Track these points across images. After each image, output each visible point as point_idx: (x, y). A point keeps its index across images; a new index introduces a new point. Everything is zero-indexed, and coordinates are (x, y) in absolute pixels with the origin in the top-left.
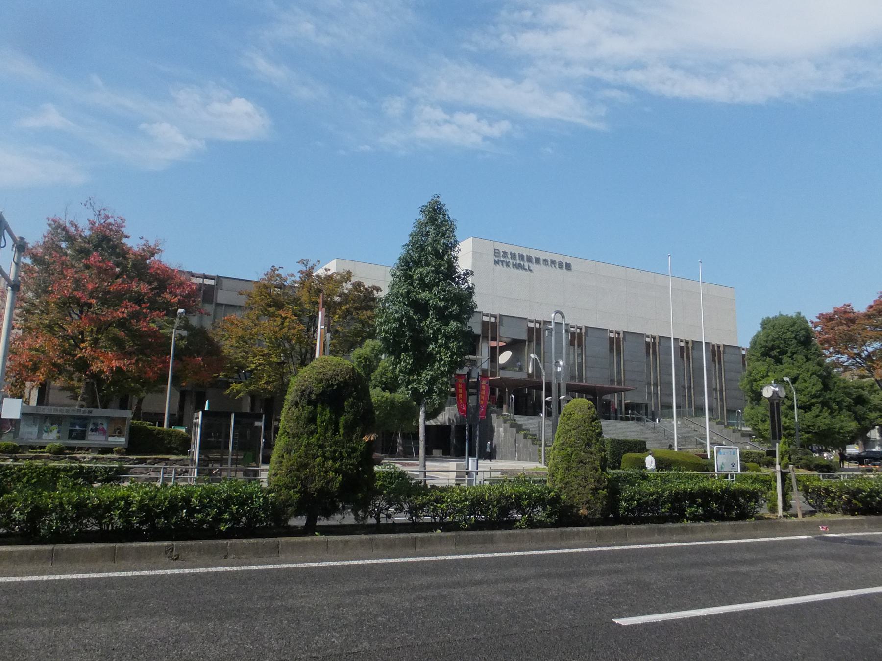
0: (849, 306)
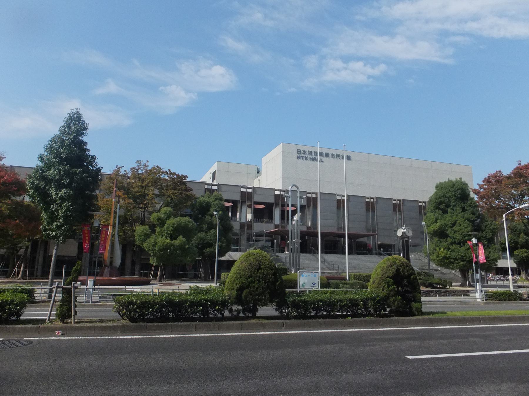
0: (500, 172)
